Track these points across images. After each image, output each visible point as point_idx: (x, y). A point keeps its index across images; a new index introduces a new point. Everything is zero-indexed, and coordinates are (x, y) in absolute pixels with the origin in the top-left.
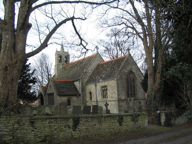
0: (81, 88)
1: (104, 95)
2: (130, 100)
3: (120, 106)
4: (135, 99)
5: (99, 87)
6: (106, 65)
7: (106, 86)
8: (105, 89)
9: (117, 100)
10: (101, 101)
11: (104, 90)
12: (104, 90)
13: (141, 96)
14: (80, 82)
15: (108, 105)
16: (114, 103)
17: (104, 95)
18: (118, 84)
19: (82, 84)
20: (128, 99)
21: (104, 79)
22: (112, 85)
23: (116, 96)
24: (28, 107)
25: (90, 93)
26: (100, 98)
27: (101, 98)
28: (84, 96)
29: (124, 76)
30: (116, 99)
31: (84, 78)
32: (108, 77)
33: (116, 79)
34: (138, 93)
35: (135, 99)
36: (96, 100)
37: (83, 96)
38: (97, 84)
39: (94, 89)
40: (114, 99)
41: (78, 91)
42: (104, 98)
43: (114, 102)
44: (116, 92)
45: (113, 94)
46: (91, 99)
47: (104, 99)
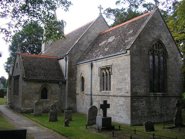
0: (67, 69)
1: (105, 84)
2: (155, 97)
3: (133, 109)
4: (164, 96)
5: (96, 70)
6: (106, 47)
7: (108, 68)
8: (106, 73)
9: (129, 94)
10: (99, 94)
11: (106, 75)
12: (106, 75)
13: (174, 90)
14: (66, 60)
15: (108, 106)
16: (122, 101)
17: (105, 84)
18: (132, 63)
19: (70, 63)
20: (152, 94)
21: (106, 55)
22: (121, 65)
23: (128, 87)
24: (78, 107)
25: (83, 78)
26: (97, 87)
27: (99, 89)
28: (72, 85)
29: (145, 49)
30: (127, 92)
31: (75, 54)
32: (115, 50)
33: (128, 51)
34: (169, 84)
35: (164, 96)
36: (90, 93)
37: (70, 85)
38: (94, 63)
39: (89, 72)
40: (123, 93)
41: (63, 76)
42: (103, 90)
43: (123, 99)
44: (129, 79)
45: (122, 82)
46: (83, 89)
47: (104, 91)
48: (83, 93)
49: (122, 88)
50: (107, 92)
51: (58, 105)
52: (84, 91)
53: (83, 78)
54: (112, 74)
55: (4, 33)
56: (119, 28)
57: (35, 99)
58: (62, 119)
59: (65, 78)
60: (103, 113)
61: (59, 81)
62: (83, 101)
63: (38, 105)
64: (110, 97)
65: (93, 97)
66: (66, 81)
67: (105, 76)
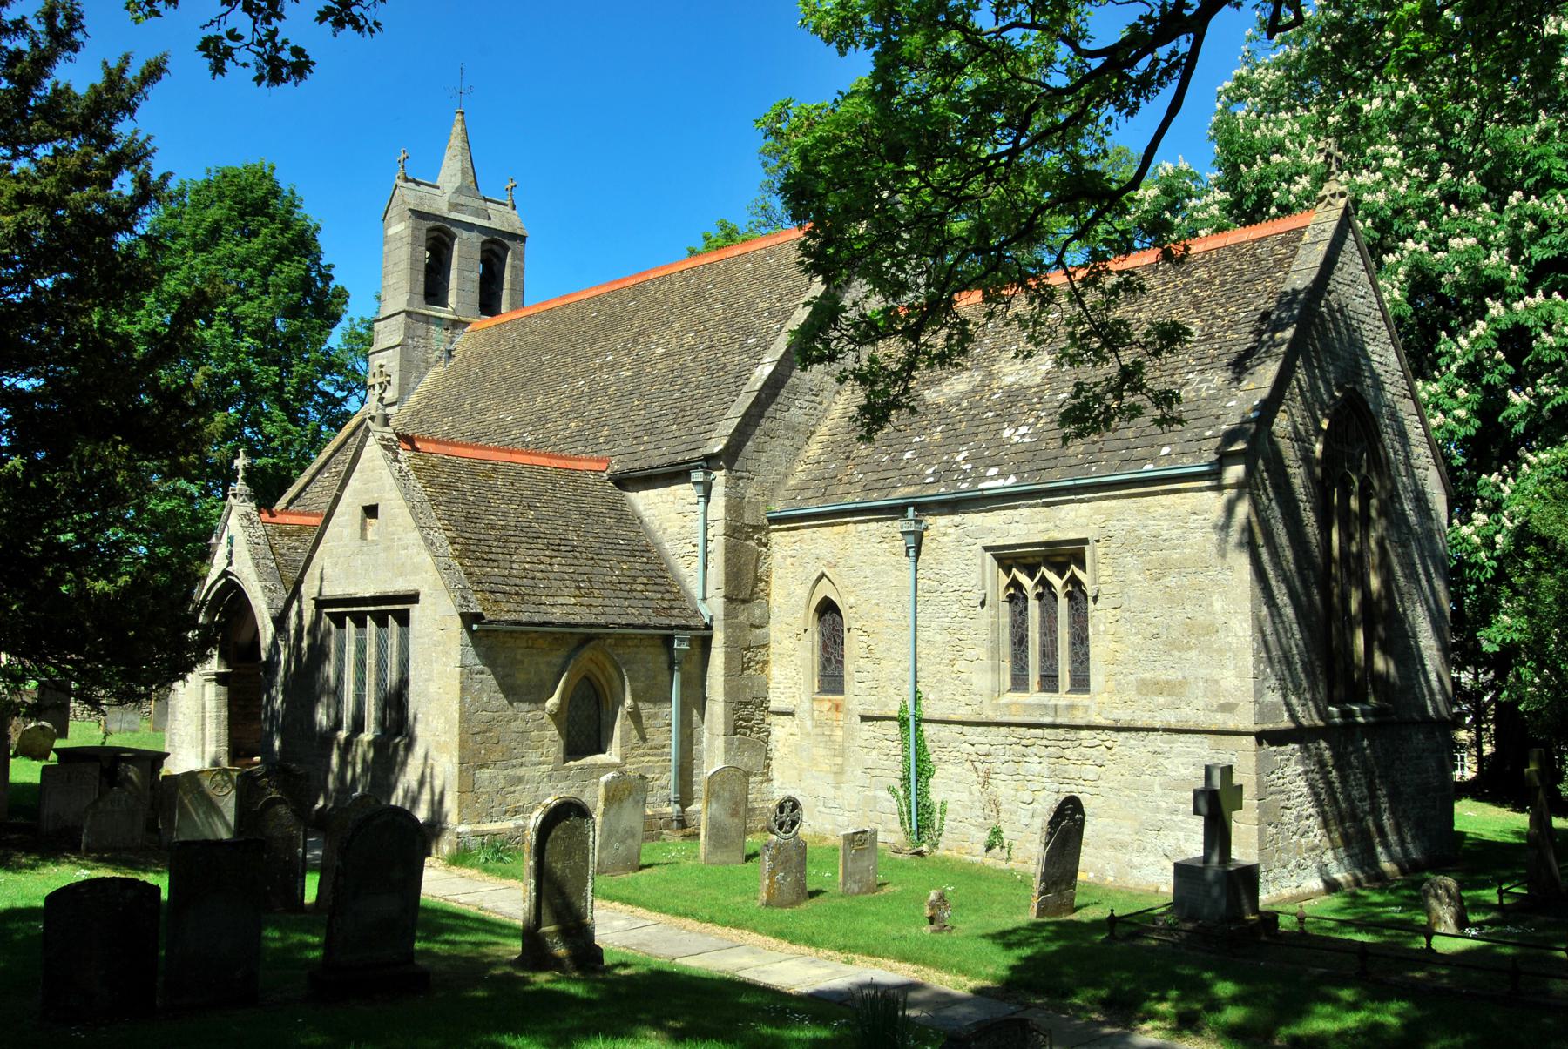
48: (837, 707)
49: (1184, 682)
50: (1062, 698)
51: (727, 795)
52: (842, 693)
53: (828, 609)
54: (1095, 599)
55: (285, 42)
56: (532, 467)
57: (533, 756)
58: (935, 927)
59: (703, 608)
60: (225, 712)
61: (670, 627)
62: (839, 761)
63: (621, 800)
64: (1084, 733)
65: (929, 730)
66: (709, 627)
67: (1034, 607)
